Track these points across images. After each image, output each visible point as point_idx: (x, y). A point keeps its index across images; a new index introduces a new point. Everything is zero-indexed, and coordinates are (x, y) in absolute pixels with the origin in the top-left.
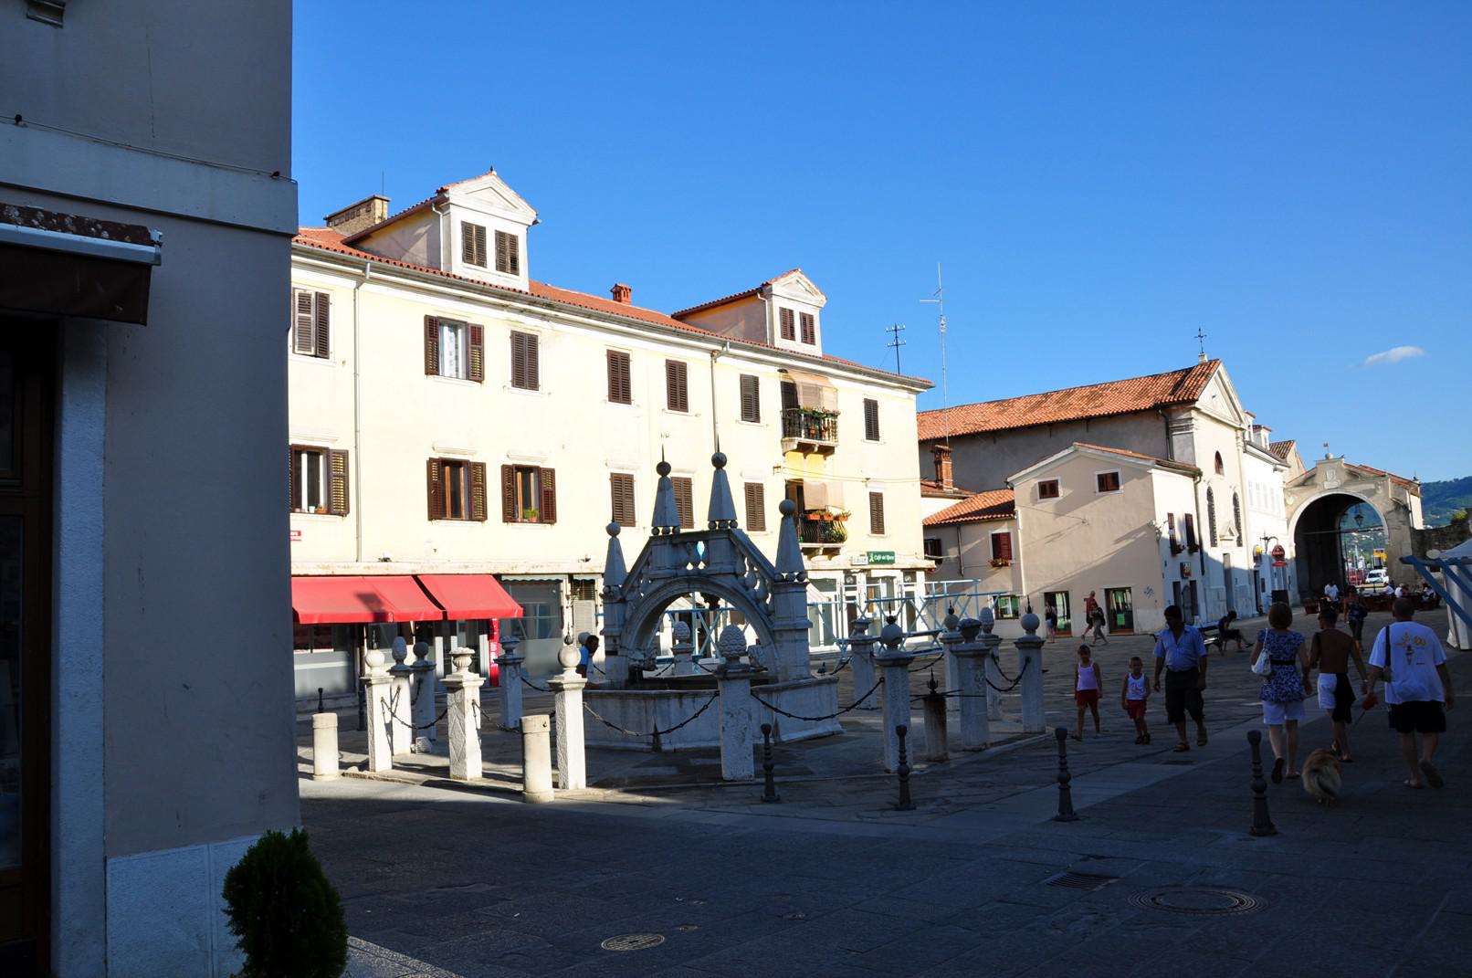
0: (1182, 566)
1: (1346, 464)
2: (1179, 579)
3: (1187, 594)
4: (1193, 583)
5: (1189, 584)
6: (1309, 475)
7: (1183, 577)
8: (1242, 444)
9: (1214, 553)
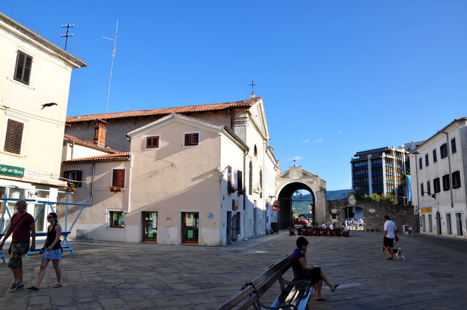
0: (233, 201)
1: (302, 170)
2: (231, 210)
3: (235, 221)
4: (238, 213)
5: (236, 213)
6: (286, 173)
7: (233, 209)
8: (265, 147)
9: (251, 198)
